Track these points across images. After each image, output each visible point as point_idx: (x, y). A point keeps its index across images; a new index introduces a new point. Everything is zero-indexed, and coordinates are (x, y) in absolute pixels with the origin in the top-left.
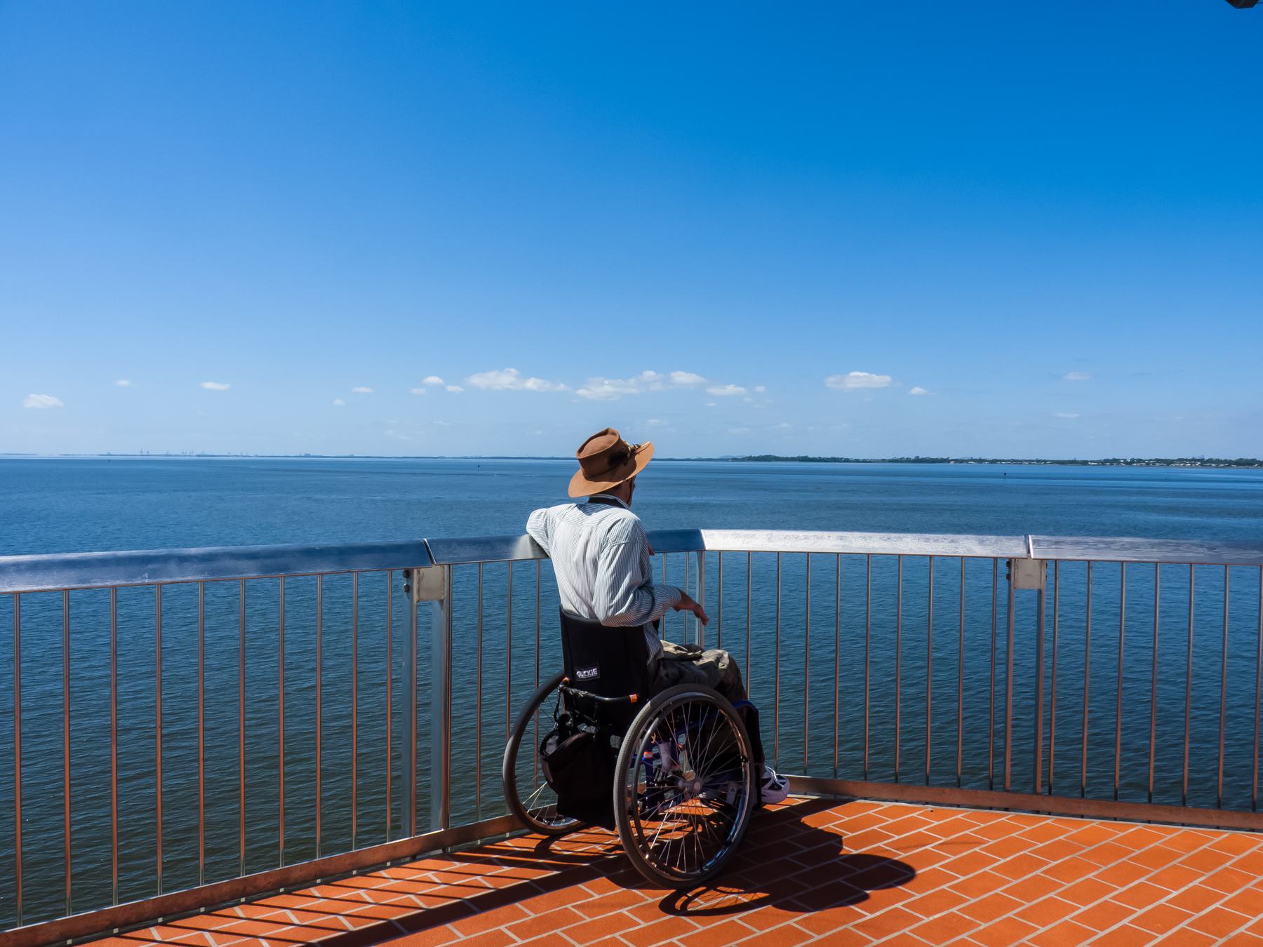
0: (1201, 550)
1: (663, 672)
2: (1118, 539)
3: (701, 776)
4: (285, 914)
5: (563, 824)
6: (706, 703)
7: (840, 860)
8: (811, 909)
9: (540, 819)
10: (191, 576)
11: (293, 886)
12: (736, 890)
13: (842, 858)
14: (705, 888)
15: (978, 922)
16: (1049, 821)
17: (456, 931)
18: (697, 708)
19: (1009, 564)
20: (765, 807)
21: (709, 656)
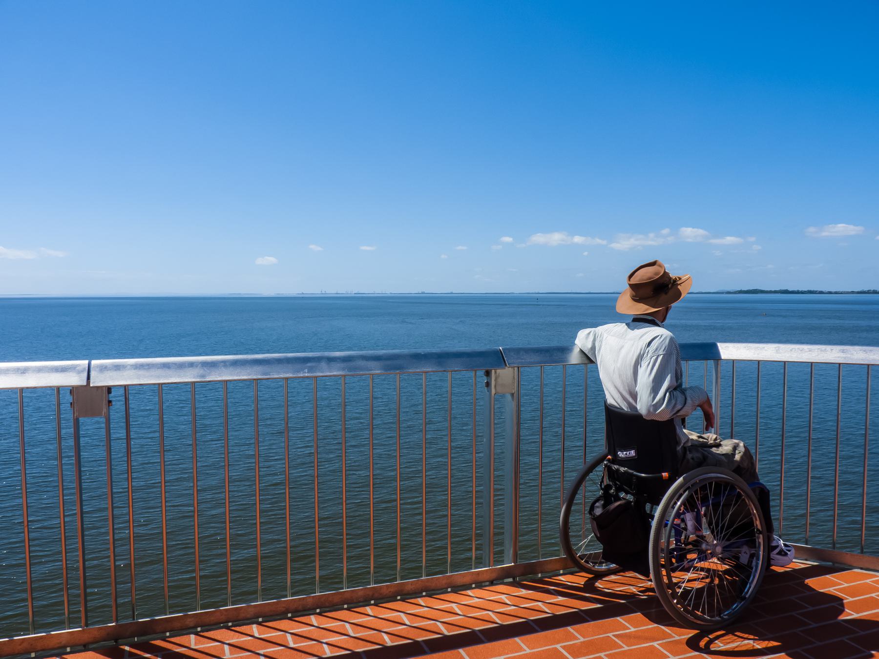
1: (689, 456)
3: (720, 541)
4: (400, 615)
5: (604, 567)
6: (727, 484)
9: (587, 562)
10: (336, 371)
11: (407, 595)
12: (752, 637)
14: (724, 632)
17: (523, 645)
18: (720, 487)
21: (726, 447)
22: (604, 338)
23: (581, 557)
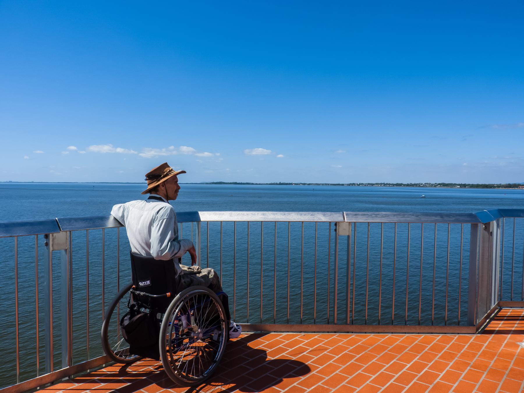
0: (413, 217)
1: (183, 281)
2: (380, 213)
7: (267, 364)
8: (255, 390)
12: (220, 384)
13: (267, 362)
14: (205, 384)
15: (331, 388)
16: (353, 336)
18: (201, 297)
19: (336, 224)
20: (230, 340)
21: (204, 272)
22: (130, 209)
23: (117, 354)
